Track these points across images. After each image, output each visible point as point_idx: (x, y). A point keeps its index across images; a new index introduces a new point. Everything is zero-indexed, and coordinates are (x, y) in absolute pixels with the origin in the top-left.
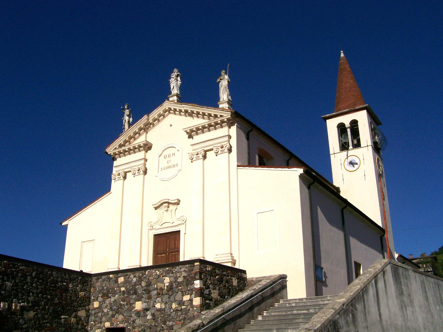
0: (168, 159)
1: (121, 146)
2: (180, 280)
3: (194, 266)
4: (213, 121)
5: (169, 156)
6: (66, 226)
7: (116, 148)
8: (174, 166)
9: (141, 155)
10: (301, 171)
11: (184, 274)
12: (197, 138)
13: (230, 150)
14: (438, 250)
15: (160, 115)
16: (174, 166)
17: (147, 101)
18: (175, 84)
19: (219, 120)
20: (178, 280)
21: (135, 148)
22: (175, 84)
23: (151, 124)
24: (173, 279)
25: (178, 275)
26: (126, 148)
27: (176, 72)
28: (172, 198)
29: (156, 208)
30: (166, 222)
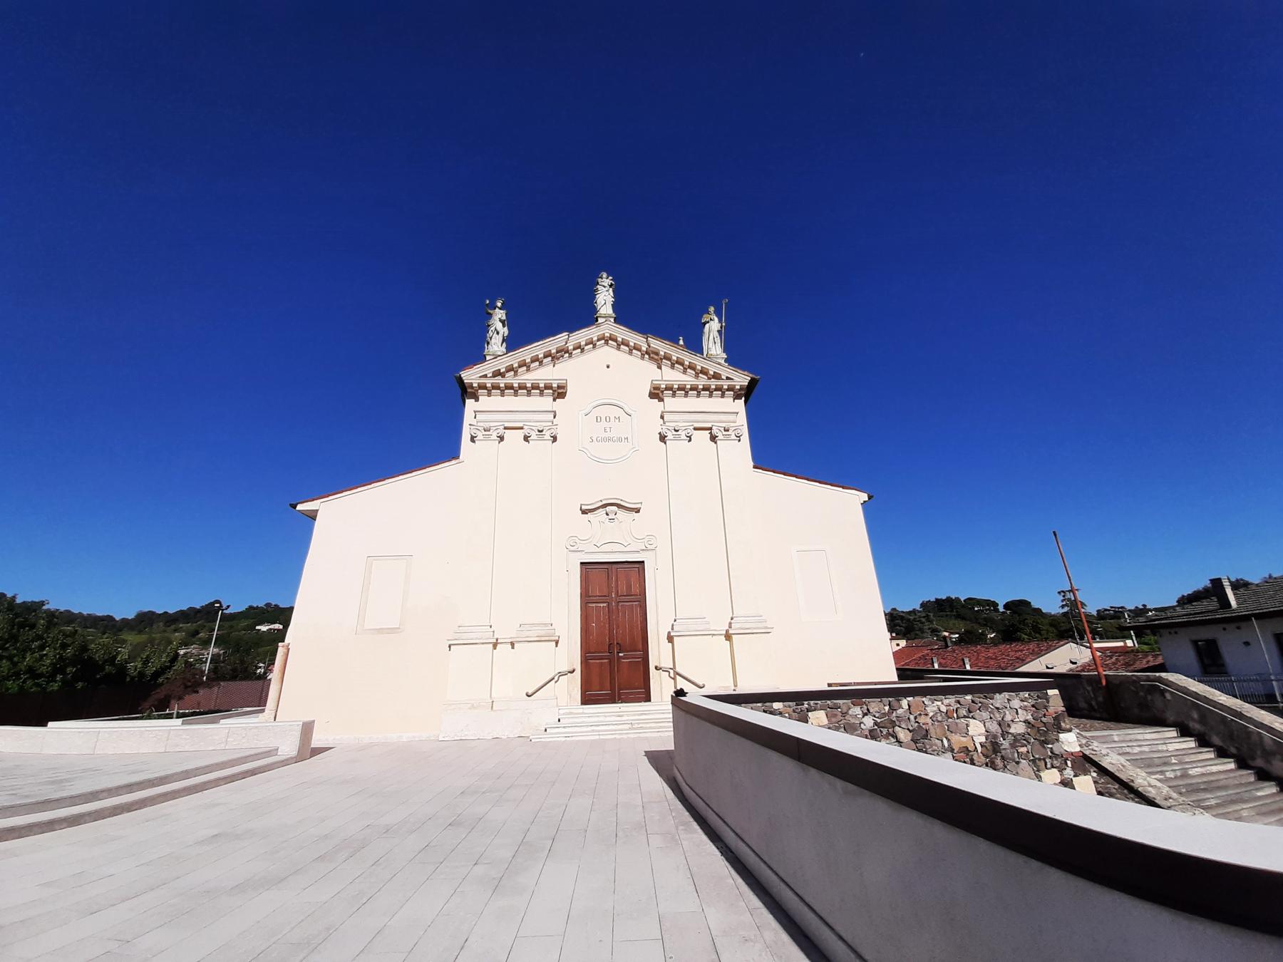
0: (604, 424)
1: (497, 373)
2: (1018, 728)
3: (1047, 698)
4: (702, 381)
5: (608, 419)
6: (312, 516)
7: (485, 376)
8: (620, 440)
9: (546, 402)
10: (865, 497)
11: (1023, 715)
12: (671, 403)
13: (739, 438)
14: (918, 608)
15: (625, 343)
16: (620, 440)
17: (552, 312)
18: (605, 299)
19: (713, 383)
20: (1012, 731)
21: (511, 387)
22: (605, 299)
23: (567, 352)
24: (994, 727)
25: (1008, 718)
26: (502, 382)
27: (605, 281)
28: (629, 501)
29: (584, 512)
30: (612, 542)
